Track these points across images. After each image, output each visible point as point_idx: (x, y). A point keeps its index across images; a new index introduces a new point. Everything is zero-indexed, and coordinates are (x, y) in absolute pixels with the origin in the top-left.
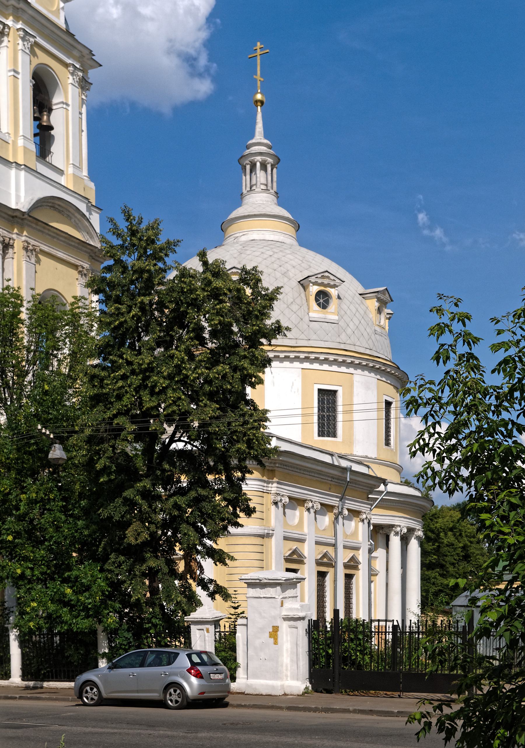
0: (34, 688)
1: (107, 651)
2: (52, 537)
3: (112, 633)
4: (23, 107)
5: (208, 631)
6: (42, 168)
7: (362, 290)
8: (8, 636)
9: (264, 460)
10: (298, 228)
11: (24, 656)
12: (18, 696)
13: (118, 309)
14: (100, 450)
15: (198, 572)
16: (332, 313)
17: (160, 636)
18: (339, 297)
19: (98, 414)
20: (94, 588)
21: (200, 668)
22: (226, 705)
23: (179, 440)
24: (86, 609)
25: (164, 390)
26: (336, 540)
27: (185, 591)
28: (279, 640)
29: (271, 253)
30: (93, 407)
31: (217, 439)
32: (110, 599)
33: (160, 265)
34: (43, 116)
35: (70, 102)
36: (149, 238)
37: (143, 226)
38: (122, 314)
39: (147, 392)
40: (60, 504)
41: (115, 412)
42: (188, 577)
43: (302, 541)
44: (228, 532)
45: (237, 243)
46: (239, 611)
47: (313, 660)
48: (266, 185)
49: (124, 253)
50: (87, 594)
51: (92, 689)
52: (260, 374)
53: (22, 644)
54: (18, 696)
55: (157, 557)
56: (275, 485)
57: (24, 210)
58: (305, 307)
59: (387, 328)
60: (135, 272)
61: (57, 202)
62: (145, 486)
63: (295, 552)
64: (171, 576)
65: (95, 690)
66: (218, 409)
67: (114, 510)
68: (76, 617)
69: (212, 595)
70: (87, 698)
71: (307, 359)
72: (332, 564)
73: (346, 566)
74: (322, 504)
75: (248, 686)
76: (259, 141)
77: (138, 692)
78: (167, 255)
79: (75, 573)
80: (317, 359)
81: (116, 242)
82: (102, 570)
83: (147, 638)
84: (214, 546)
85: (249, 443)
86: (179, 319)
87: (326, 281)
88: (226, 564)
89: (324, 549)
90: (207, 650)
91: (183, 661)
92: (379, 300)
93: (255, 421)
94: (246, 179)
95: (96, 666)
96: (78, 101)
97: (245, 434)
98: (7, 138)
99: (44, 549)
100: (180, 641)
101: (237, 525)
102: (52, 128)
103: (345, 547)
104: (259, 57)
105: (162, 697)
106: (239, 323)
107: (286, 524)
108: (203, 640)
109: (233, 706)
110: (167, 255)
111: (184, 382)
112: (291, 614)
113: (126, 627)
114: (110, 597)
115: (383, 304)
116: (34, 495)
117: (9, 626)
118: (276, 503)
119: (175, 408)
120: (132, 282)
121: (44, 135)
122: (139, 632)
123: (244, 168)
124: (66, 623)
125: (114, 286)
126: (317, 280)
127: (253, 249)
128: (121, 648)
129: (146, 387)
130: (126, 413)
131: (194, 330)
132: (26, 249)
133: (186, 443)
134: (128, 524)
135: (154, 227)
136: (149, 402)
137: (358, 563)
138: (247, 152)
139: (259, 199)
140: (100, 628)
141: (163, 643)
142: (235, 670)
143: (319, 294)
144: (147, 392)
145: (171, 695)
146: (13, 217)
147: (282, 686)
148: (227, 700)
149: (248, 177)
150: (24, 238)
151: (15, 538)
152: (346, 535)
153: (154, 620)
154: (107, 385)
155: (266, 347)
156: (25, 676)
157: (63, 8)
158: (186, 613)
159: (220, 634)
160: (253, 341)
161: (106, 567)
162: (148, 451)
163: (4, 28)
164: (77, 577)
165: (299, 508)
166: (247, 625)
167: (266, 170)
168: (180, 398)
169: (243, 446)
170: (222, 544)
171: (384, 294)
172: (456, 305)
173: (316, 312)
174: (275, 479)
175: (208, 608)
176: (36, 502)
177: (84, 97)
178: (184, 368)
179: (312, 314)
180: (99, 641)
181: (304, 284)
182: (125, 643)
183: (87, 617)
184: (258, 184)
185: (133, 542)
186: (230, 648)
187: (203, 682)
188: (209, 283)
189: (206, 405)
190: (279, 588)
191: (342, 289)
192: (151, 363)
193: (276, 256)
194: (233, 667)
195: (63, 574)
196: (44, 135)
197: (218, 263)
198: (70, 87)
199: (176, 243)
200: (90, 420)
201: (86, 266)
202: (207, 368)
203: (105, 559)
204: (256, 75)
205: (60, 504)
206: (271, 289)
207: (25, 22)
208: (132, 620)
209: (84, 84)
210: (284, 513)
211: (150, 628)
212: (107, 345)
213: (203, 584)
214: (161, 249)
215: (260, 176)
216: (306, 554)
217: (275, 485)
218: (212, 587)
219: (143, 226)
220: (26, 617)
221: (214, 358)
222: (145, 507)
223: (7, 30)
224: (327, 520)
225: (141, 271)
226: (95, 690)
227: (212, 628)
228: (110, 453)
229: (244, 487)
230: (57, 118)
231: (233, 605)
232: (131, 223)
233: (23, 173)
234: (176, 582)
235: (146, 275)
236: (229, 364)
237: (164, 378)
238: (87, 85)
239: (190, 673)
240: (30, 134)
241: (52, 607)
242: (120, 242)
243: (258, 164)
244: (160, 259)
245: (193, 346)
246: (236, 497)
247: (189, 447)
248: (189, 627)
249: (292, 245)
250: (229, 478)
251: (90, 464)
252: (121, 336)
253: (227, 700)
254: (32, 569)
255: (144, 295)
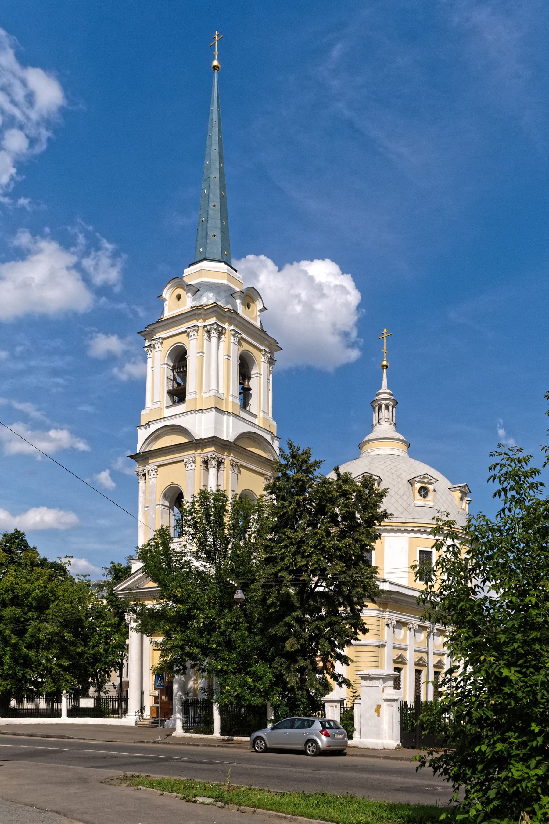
0: (228, 740)
1: (273, 718)
2: (239, 646)
3: (276, 708)
4: (233, 377)
5: (336, 707)
6: (243, 415)
7: (450, 485)
8: (213, 707)
9: (375, 599)
10: (409, 446)
11: (222, 719)
12: (217, 745)
13: (283, 504)
14: (270, 592)
15: (331, 670)
16: (429, 501)
17: (306, 710)
18: (434, 491)
19: (270, 569)
20: (265, 679)
21: (328, 730)
22: (345, 754)
23: (321, 586)
24: (260, 692)
25: (310, 555)
26: (428, 649)
27: (322, 681)
28: (381, 714)
29: (390, 463)
30: (266, 565)
31: (344, 585)
32: (276, 686)
33: (310, 476)
34: (245, 382)
35: (262, 373)
36: (303, 460)
37: (300, 452)
38: (286, 507)
39: (300, 556)
40: (246, 625)
41: (279, 568)
42: (325, 672)
43: (405, 649)
44: (351, 644)
45: (369, 456)
46: (357, 694)
47: (403, 729)
48: (389, 419)
49: (288, 469)
50: (260, 682)
51: (261, 742)
52: (373, 544)
53: (221, 713)
54: (217, 745)
55: (305, 660)
56: (388, 613)
57: (231, 441)
58: (412, 497)
59: (467, 510)
60: (294, 481)
61: (252, 435)
62: (298, 615)
63: (400, 657)
64: (314, 672)
65: (263, 742)
66: (345, 566)
67: (278, 630)
68: (254, 696)
69: (340, 684)
70: (258, 747)
71: (412, 531)
72: (425, 665)
73: (435, 666)
74: (419, 626)
75: (360, 743)
76: (384, 391)
77: (289, 744)
78: (314, 470)
79: (253, 669)
80: (419, 531)
81: (283, 462)
82: (270, 667)
83: (298, 710)
84: (342, 653)
85: (364, 588)
86: (321, 510)
87: (426, 480)
88: (349, 665)
89: (420, 655)
90: (335, 720)
91: (317, 726)
92: (461, 492)
93: (368, 573)
94: (375, 416)
95: (266, 727)
96: (267, 371)
97: (362, 582)
98: (222, 397)
99: (235, 654)
100: (319, 713)
101: (357, 639)
102: (250, 389)
103: (434, 654)
104: (385, 338)
105: (304, 748)
106: (360, 512)
107: (394, 638)
108: (333, 713)
109: (349, 755)
110: (314, 470)
111: (323, 550)
112: (389, 697)
113: (285, 703)
114: (276, 684)
115: (464, 494)
116: (229, 620)
117: (214, 701)
118: (388, 625)
119: (317, 566)
120: (292, 487)
121: (245, 394)
122: (293, 706)
123: (374, 408)
124: (248, 700)
125: (281, 490)
126: (420, 480)
127: (379, 460)
128: (282, 717)
129: (299, 552)
130: (286, 569)
131: (330, 517)
132: (232, 465)
133: (325, 587)
134: (287, 638)
135: (307, 453)
136: (301, 562)
137: (443, 664)
138: (377, 398)
139: (384, 427)
140: (269, 704)
141: (308, 714)
142: (353, 732)
143: (421, 488)
144: (300, 556)
145: (309, 747)
146: (225, 445)
147: (382, 743)
148: (345, 751)
149: (377, 414)
150: (231, 458)
151: (217, 646)
152: (435, 646)
153: (302, 699)
154: (275, 551)
155: (377, 526)
156: (222, 733)
157: (259, 315)
158: (323, 695)
159: (344, 709)
160: (369, 523)
161: (273, 665)
162: (300, 593)
163: (222, 330)
164: (255, 672)
165: (404, 628)
166: (360, 704)
167: (388, 410)
168: (320, 560)
169: (360, 590)
170: (346, 651)
171: (465, 488)
172: (447, 516)
173: (419, 500)
174: (388, 610)
175: (339, 692)
176: (231, 624)
177: (271, 369)
178: (324, 541)
179: (416, 502)
180: (268, 712)
181: (411, 482)
182: (284, 713)
183: (261, 696)
184: (383, 418)
185: (289, 649)
186: (350, 718)
187: (329, 739)
188: (340, 487)
189: (337, 564)
190: (381, 680)
191: (436, 485)
192: (303, 537)
193: (393, 464)
194: (351, 730)
195: (247, 669)
196: (245, 394)
197: (347, 475)
198: (262, 363)
199: (321, 462)
200: (263, 575)
201: (270, 474)
202: (338, 541)
203: (272, 660)
204: (383, 349)
205: (246, 625)
206: (381, 490)
207: (235, 326)
208: (289, 699)
209: (271, 361)
210: (394, 632)
211: (300, 704)
212: (276, 526)
213: (335, 677)
214: (311, 466)
215: (385, 413)
216: (408, 657)
217: (388, 613)
218: (340, 679)
219: (300, 452)
220: (223, 696)
221: (343, 535)
222: (298, 628)
223: (224, 331)
224: (422, 636)
225: (297, 480)
226: (263, 742)
227: (338, 705)
228: (276, 594)
229: (361, 615)
230: (253, 383)
231: (353, 691)
232: (293, 450)
233: (231, 418)
234: (317, 675)
235: (300, 483)
236: (353, 538)
237: (311, 547)
238: (273, 361)
239: (322, 733)
240: (236, 394)
241: (239, 690)
242: (285, 462)
243: (383, 406)
244: (310, 472)
245: (330, 527)
246: (356, 622)
247: (327, 589)
248: (324, 705)
249: (405, 457)
250: (353, 610)
251: (263, 601)
252: (286, 521)
253: (345, 751)
254: (227, 666)
255: (299, 495)
